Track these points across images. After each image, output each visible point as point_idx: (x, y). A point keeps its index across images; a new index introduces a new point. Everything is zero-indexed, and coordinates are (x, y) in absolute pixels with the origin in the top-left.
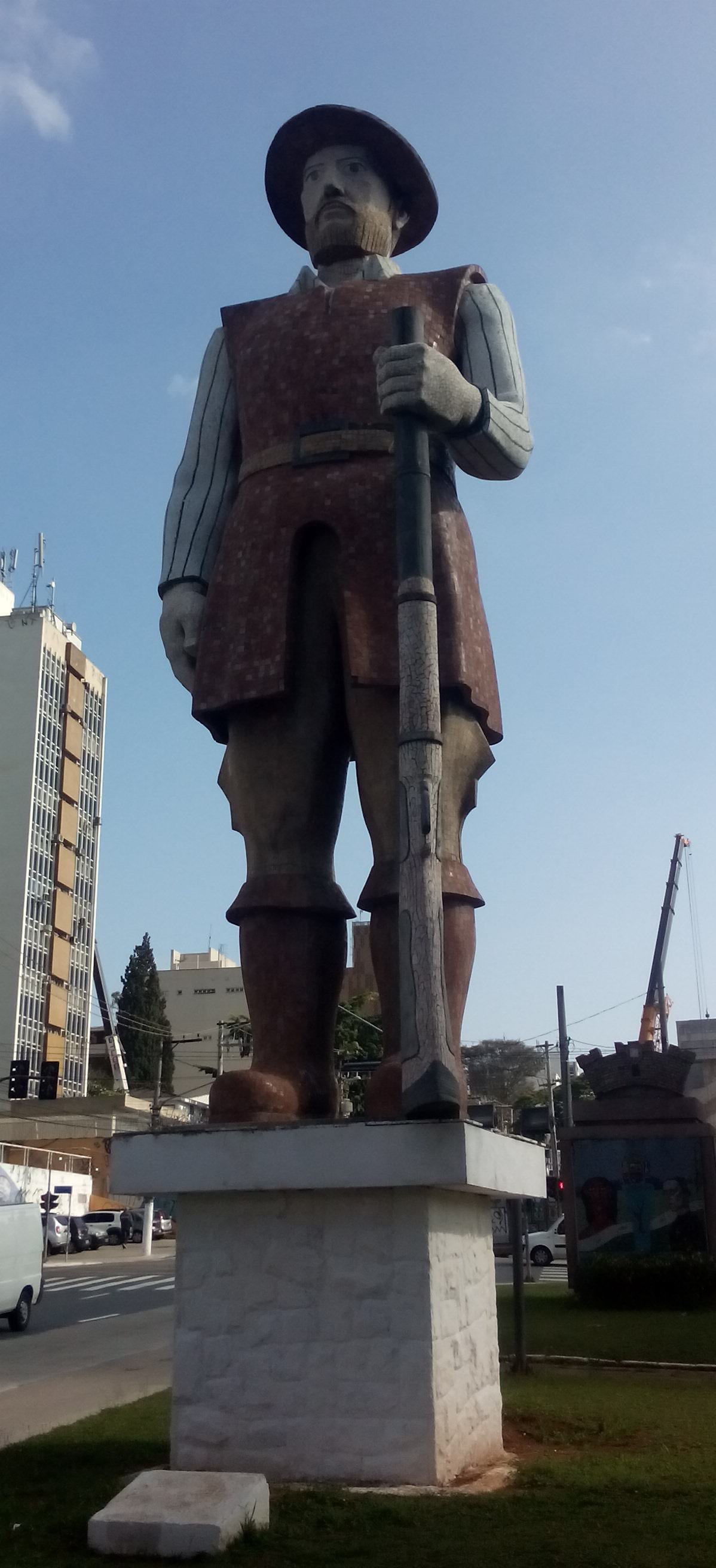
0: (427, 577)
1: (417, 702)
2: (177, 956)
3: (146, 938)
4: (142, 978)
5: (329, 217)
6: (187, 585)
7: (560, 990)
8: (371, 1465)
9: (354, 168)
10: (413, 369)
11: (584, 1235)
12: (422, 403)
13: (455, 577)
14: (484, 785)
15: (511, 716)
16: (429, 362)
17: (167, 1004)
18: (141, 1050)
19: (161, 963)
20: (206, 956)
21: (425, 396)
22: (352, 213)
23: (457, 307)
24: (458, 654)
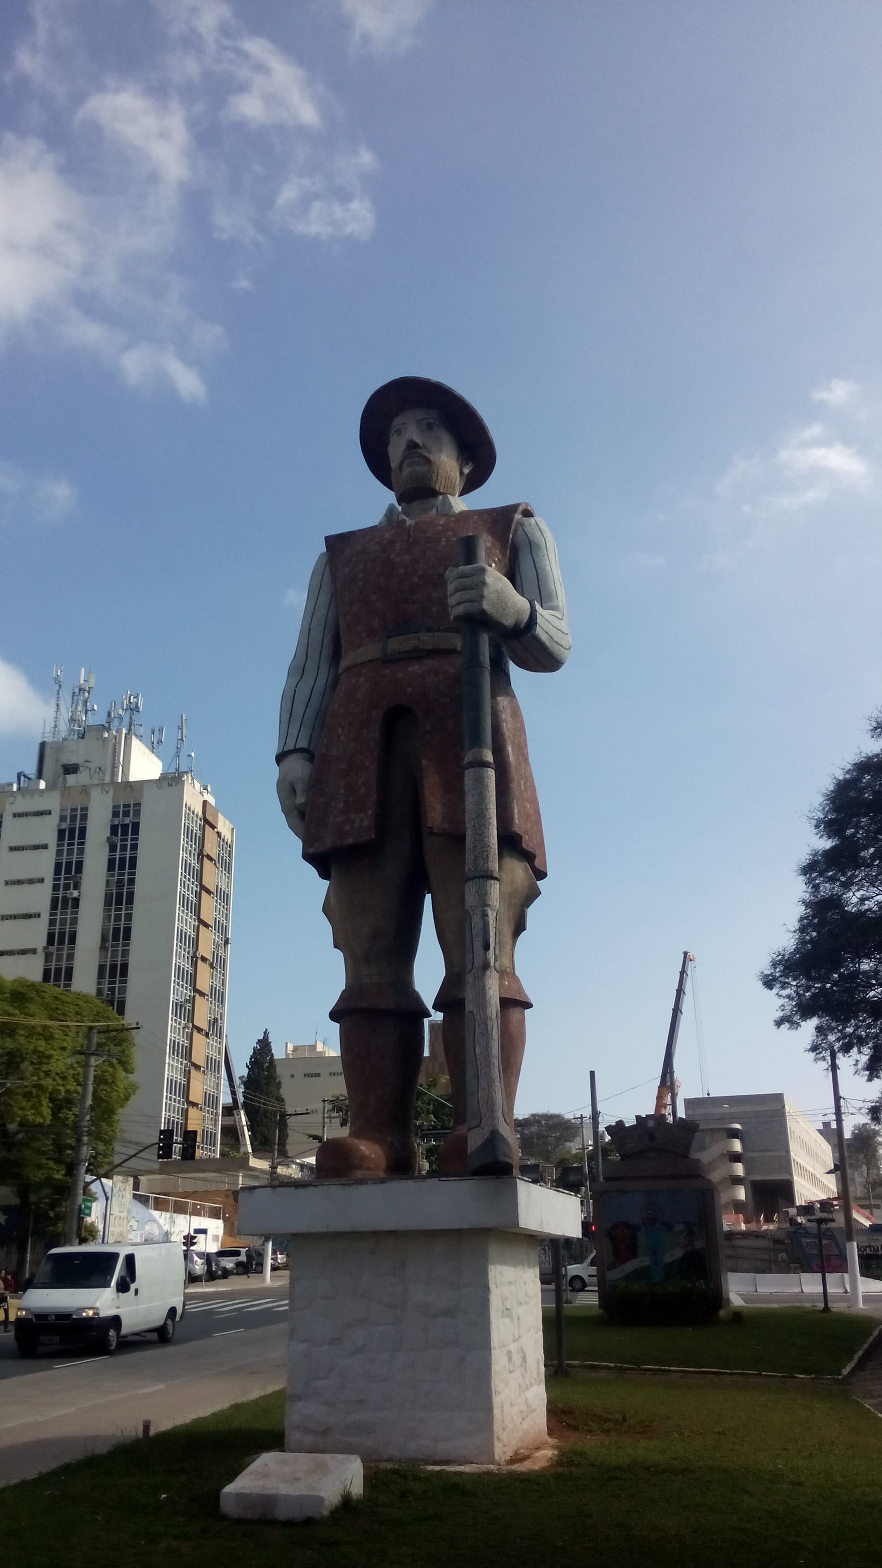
2: (290, 1047)
3: (266, 1033)
4: (263, 1064)
5: (410, 465)
6: (298, 755)
7: (592, 1074)
8: (443, 1448)
9: (430, 427)
10: (477, 585)
11: (611, 1267)
12: (483, 612)
13: (510, 749)
14: (532, 912)
15: (554, 858)
16: (489, 579)
18: (262, 1121)
19: (278, 1053)
20: (313, 1047)
21: (486, 606)
22: (428, 461)
24: (512, 809)
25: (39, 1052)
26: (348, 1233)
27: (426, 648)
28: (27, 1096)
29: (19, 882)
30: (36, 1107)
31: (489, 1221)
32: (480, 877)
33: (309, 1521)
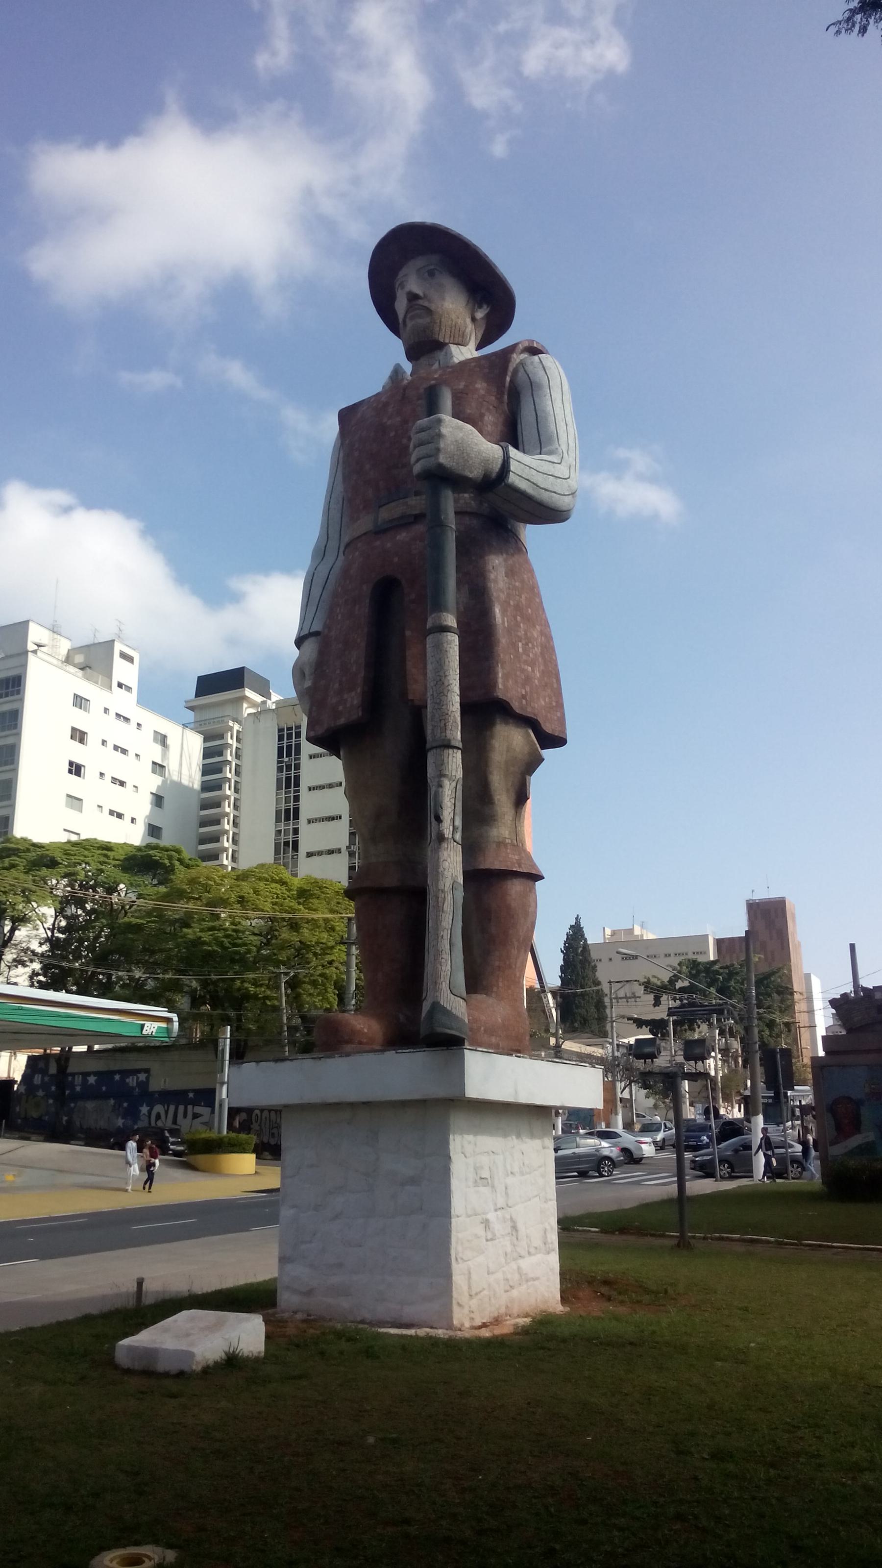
0: (447, 610)
1: (437, 716)
2: (608, 932)
3: (577, 919)
4: (577, 949)
5: (412, 318)
7: (852, 947)
8: (410, 1312)
9: (431, 274)
10: (433, 438)
11: (834, 1143)
12: (440, 466)
13: (497, 610)
16: (444, 430)
17: (598, 968)
18: (580, 1003)
19: (593, 937)
20: (631, 931)
21: (442, 459)
22: (429, 311)
23: (508, 379)
24: (496, 674)
25: (322, 943)
26: (330, 1104)
27: (414, 512)
28: (314, 983)
29: (322, 787)
30: (323, 994)
31: (440, 1092)
32: (436, 747)
33: (181, 1374)
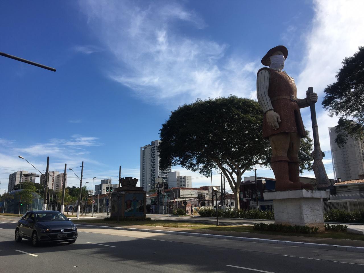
7: (120, 166)
